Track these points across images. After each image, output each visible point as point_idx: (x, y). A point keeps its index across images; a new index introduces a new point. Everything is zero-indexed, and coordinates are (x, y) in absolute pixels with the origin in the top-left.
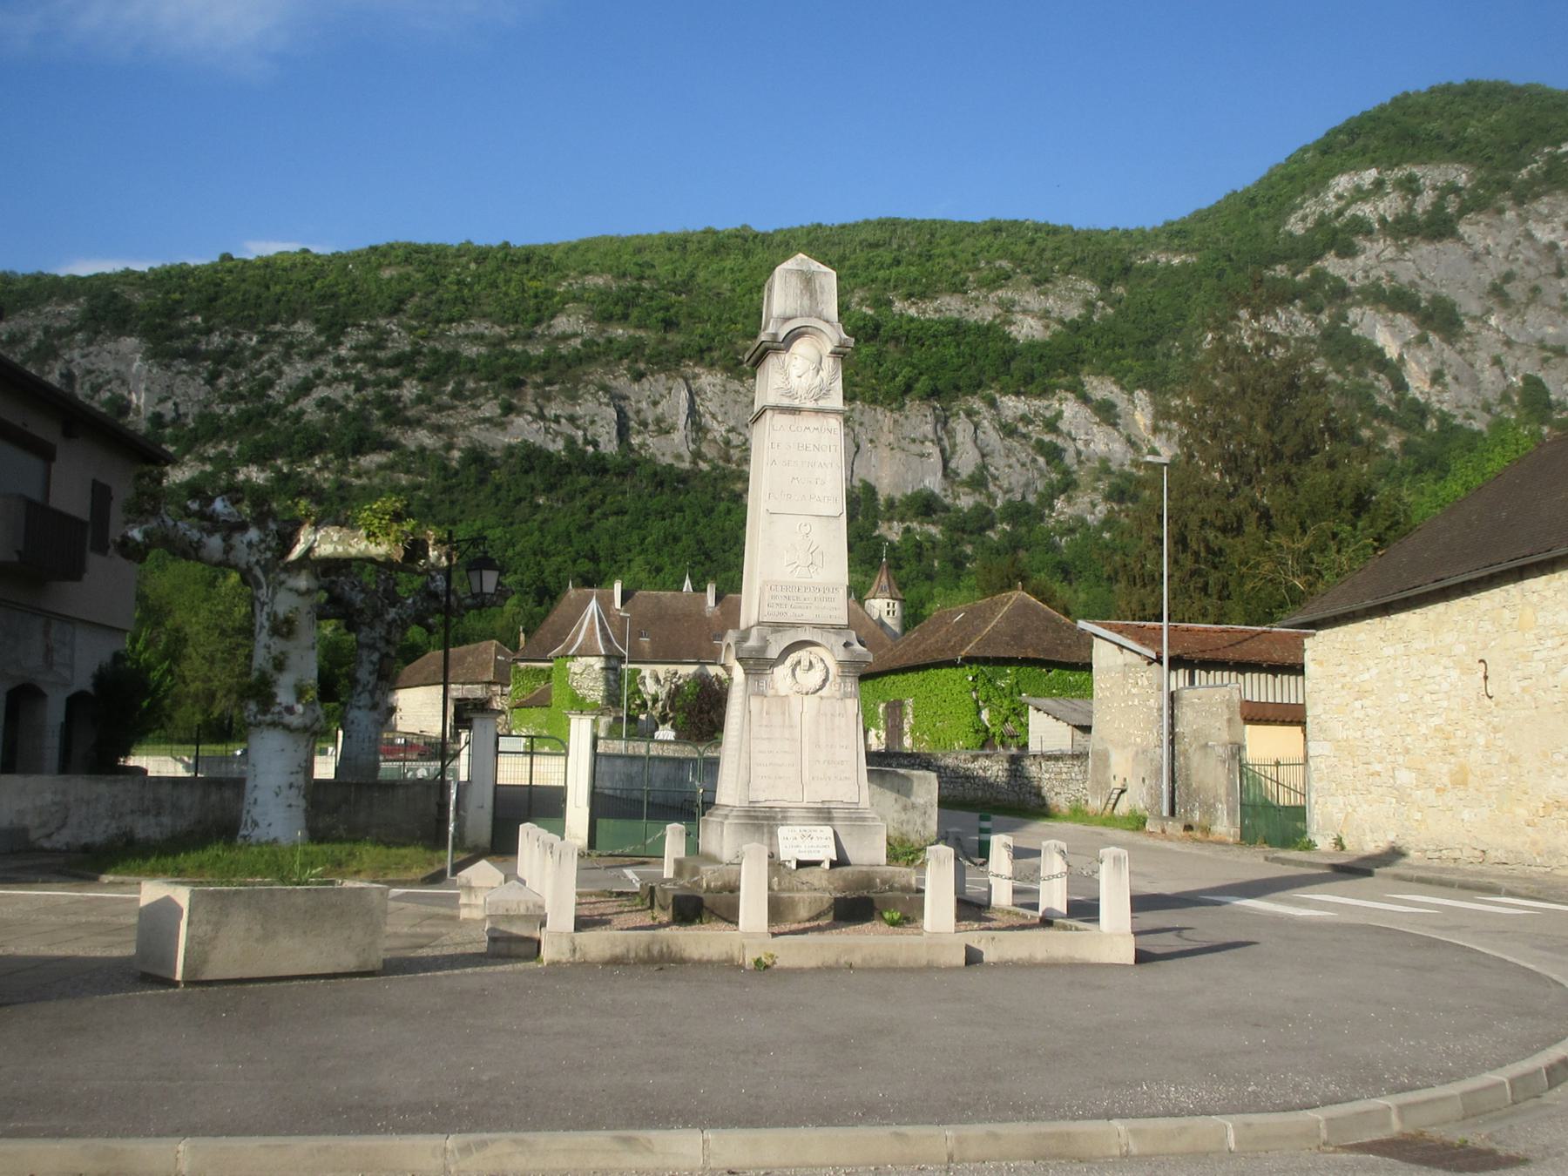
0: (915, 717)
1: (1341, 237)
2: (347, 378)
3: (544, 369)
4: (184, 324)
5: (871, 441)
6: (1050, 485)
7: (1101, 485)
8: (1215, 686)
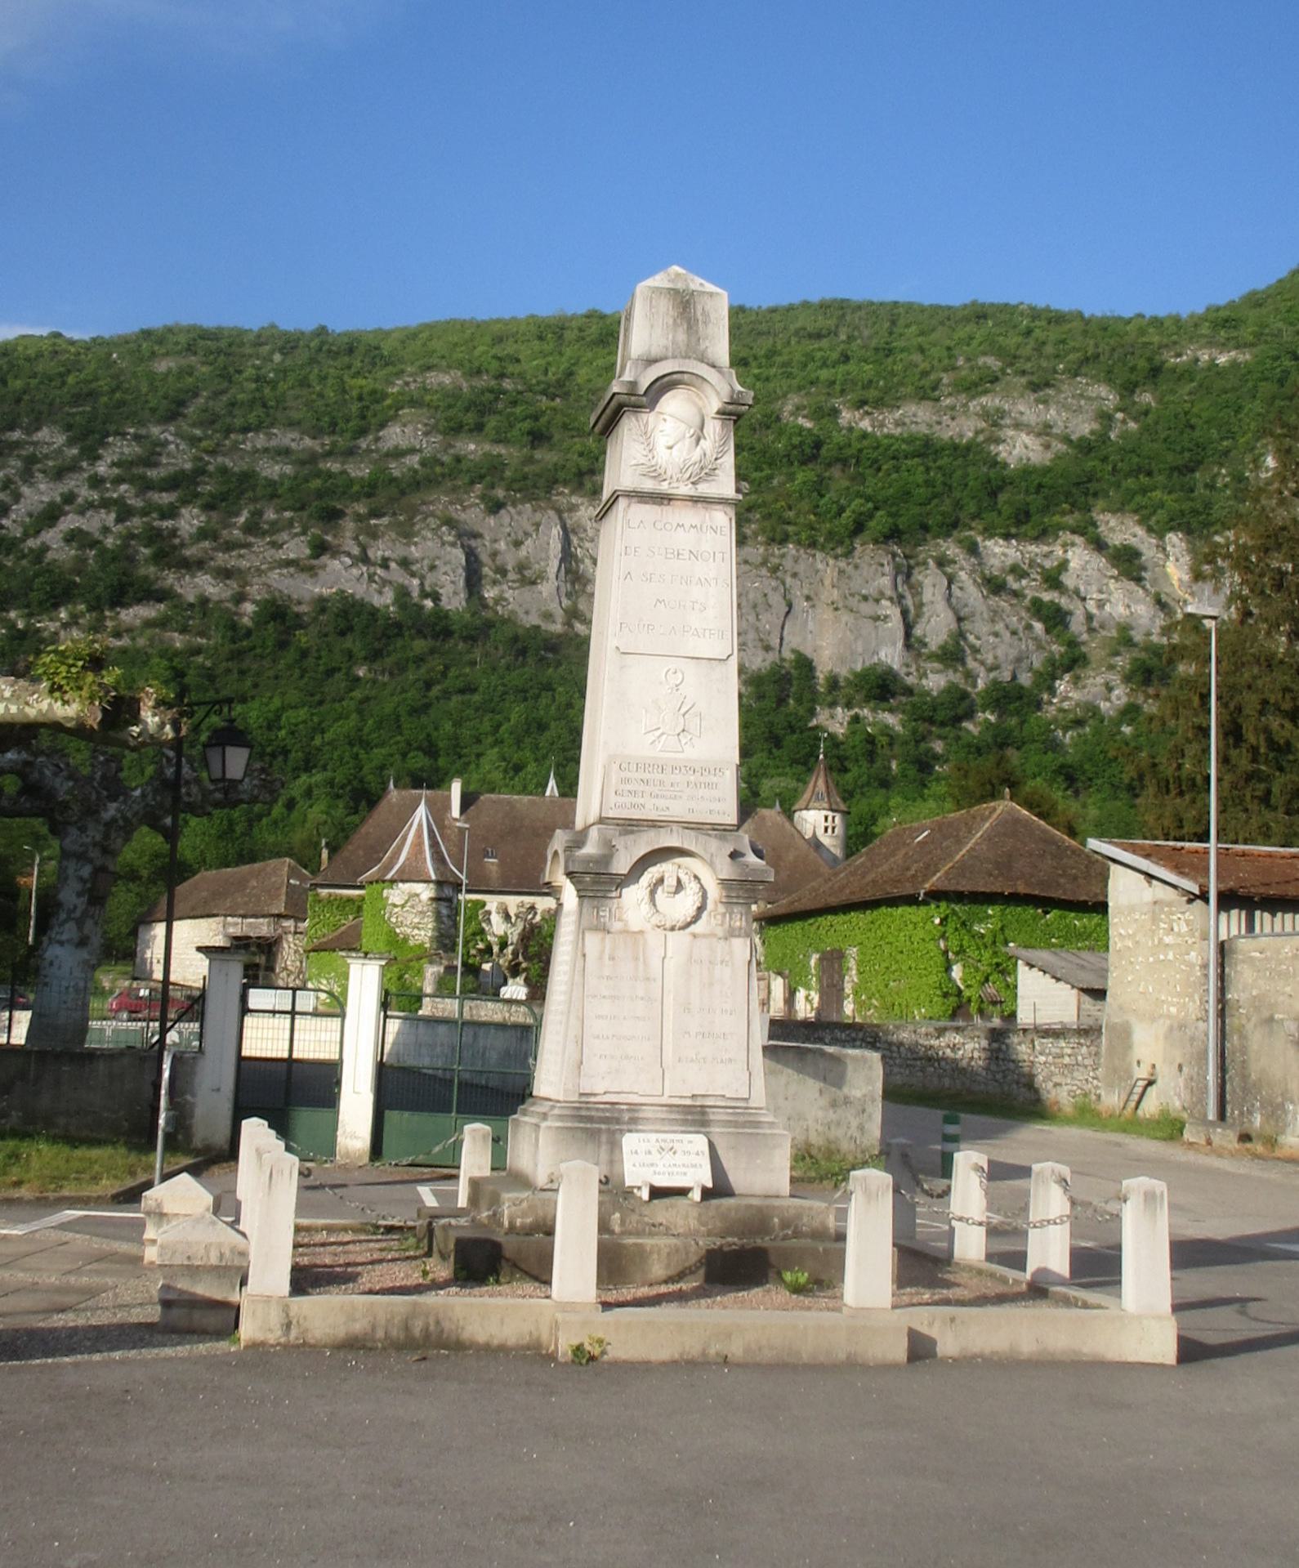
0: (860, 973)
2: (106, 504)
3: (369, 495)
5: (808, 598)
6: (1051, 661)
7: (1119, 661)
8: (1273, 934)
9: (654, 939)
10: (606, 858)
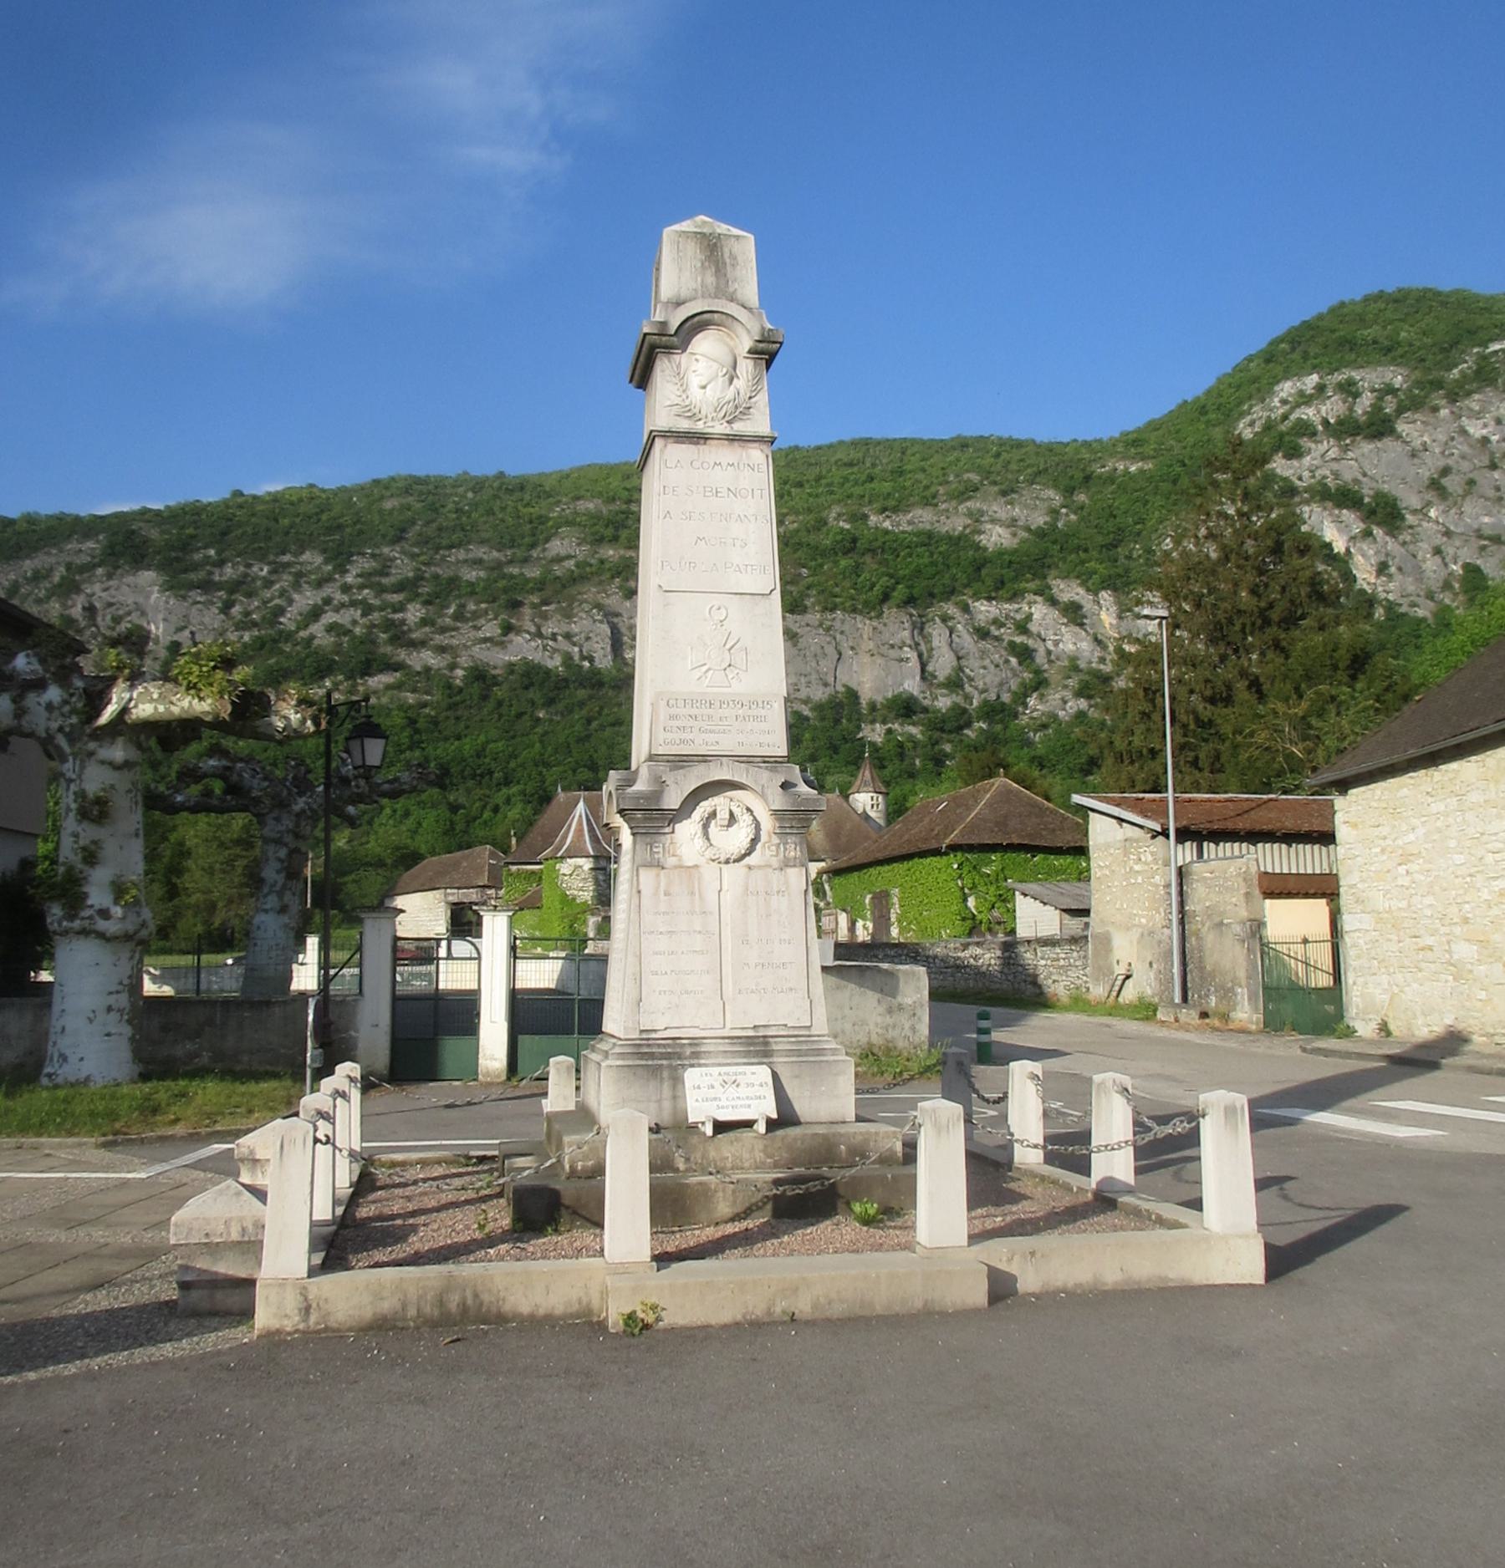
1: (1291, 439)
2: (353, 604)
3: (540, 590)
5: (852, 648)
6: (1023, 684)
7: (1070, 682)
9: (710, 872)
10: (657, 795)
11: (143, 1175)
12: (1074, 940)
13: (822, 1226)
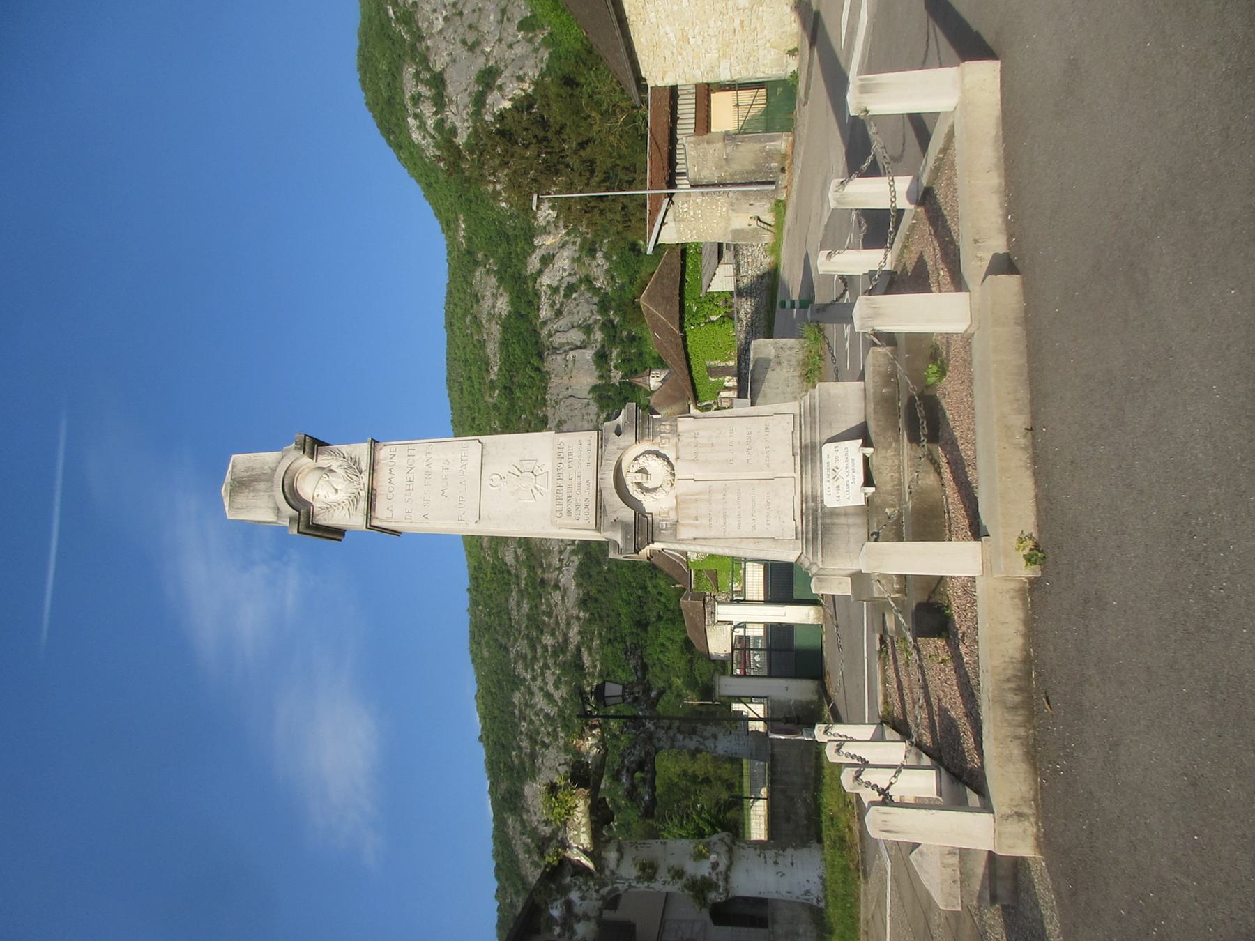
1: (446, 134)
2: (542, 674)
4: (516, 762)
6: (588, 290)
9: (680, 487)
10: (624, 526)
11: (889, 864)
12: (736, 253)
13: (945, 406)
